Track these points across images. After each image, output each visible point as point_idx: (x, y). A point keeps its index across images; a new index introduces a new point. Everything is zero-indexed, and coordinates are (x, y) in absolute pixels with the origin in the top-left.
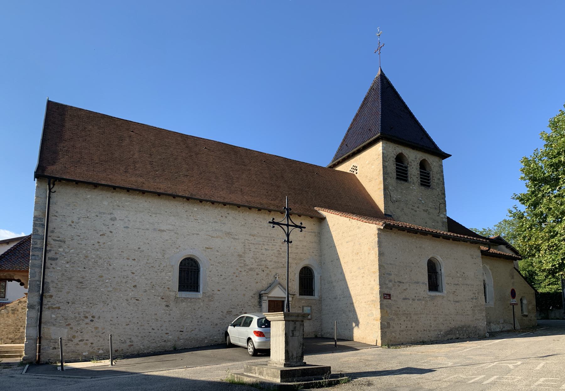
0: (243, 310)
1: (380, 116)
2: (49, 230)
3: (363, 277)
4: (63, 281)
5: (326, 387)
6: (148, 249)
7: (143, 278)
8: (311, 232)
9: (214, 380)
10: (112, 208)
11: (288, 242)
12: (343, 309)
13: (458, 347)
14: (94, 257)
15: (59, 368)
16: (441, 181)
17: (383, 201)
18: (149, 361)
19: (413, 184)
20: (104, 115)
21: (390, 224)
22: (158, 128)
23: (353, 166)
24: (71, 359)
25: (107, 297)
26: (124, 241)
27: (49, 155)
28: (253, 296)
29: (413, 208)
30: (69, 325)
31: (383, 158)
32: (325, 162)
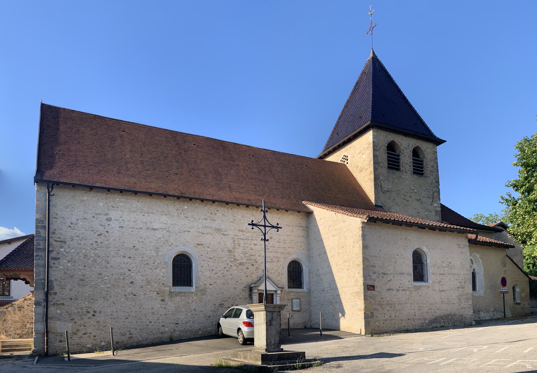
0: (234, 302)
1: (371, 102)
2: (51, 231)
3: (348, 269)
4: (65, 279)
5: (299, 369)
6: (143, 247)
7: (139, 274)
8: (299, 226)
9: (204, 365)
10: (107, 209)
11: (265, 240)
12: (330, 300)
13: (439, 334)
14: (93, 255)
15: (66, 359)
16: (435, 169)
17: (374, 191)
18: (147, 351)
19: (406, 173)
20: (96, 115)
21: (374, 217)
22: (148, 126)
23: (344, 156)
24: (76, 351)
25: (107, 293)
26: (120, 240)
27: (46, 159)
28: (244, 289)
29: (405, 197)
30: (73, 319)
31: (373, 147)
32: (314, 153)
